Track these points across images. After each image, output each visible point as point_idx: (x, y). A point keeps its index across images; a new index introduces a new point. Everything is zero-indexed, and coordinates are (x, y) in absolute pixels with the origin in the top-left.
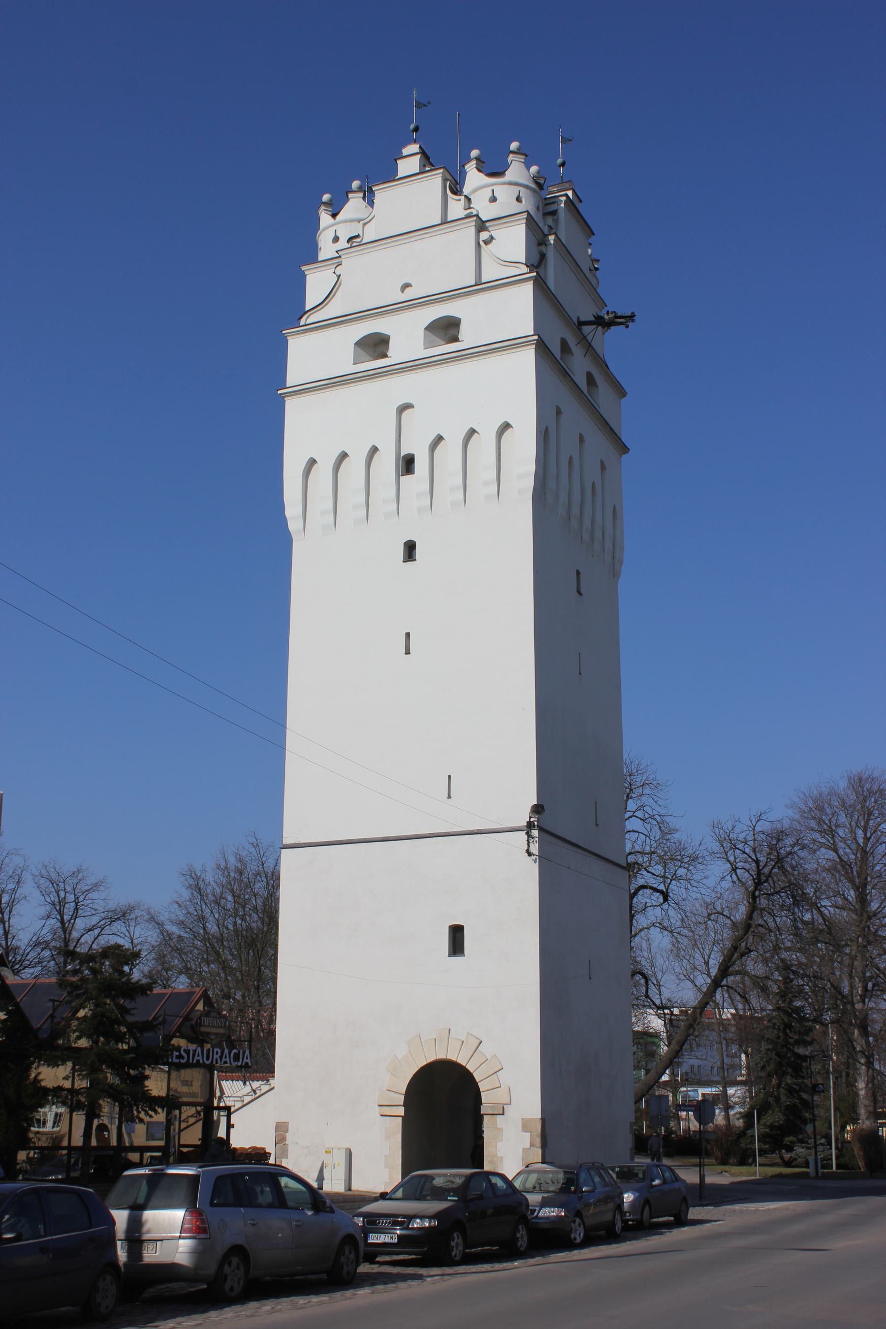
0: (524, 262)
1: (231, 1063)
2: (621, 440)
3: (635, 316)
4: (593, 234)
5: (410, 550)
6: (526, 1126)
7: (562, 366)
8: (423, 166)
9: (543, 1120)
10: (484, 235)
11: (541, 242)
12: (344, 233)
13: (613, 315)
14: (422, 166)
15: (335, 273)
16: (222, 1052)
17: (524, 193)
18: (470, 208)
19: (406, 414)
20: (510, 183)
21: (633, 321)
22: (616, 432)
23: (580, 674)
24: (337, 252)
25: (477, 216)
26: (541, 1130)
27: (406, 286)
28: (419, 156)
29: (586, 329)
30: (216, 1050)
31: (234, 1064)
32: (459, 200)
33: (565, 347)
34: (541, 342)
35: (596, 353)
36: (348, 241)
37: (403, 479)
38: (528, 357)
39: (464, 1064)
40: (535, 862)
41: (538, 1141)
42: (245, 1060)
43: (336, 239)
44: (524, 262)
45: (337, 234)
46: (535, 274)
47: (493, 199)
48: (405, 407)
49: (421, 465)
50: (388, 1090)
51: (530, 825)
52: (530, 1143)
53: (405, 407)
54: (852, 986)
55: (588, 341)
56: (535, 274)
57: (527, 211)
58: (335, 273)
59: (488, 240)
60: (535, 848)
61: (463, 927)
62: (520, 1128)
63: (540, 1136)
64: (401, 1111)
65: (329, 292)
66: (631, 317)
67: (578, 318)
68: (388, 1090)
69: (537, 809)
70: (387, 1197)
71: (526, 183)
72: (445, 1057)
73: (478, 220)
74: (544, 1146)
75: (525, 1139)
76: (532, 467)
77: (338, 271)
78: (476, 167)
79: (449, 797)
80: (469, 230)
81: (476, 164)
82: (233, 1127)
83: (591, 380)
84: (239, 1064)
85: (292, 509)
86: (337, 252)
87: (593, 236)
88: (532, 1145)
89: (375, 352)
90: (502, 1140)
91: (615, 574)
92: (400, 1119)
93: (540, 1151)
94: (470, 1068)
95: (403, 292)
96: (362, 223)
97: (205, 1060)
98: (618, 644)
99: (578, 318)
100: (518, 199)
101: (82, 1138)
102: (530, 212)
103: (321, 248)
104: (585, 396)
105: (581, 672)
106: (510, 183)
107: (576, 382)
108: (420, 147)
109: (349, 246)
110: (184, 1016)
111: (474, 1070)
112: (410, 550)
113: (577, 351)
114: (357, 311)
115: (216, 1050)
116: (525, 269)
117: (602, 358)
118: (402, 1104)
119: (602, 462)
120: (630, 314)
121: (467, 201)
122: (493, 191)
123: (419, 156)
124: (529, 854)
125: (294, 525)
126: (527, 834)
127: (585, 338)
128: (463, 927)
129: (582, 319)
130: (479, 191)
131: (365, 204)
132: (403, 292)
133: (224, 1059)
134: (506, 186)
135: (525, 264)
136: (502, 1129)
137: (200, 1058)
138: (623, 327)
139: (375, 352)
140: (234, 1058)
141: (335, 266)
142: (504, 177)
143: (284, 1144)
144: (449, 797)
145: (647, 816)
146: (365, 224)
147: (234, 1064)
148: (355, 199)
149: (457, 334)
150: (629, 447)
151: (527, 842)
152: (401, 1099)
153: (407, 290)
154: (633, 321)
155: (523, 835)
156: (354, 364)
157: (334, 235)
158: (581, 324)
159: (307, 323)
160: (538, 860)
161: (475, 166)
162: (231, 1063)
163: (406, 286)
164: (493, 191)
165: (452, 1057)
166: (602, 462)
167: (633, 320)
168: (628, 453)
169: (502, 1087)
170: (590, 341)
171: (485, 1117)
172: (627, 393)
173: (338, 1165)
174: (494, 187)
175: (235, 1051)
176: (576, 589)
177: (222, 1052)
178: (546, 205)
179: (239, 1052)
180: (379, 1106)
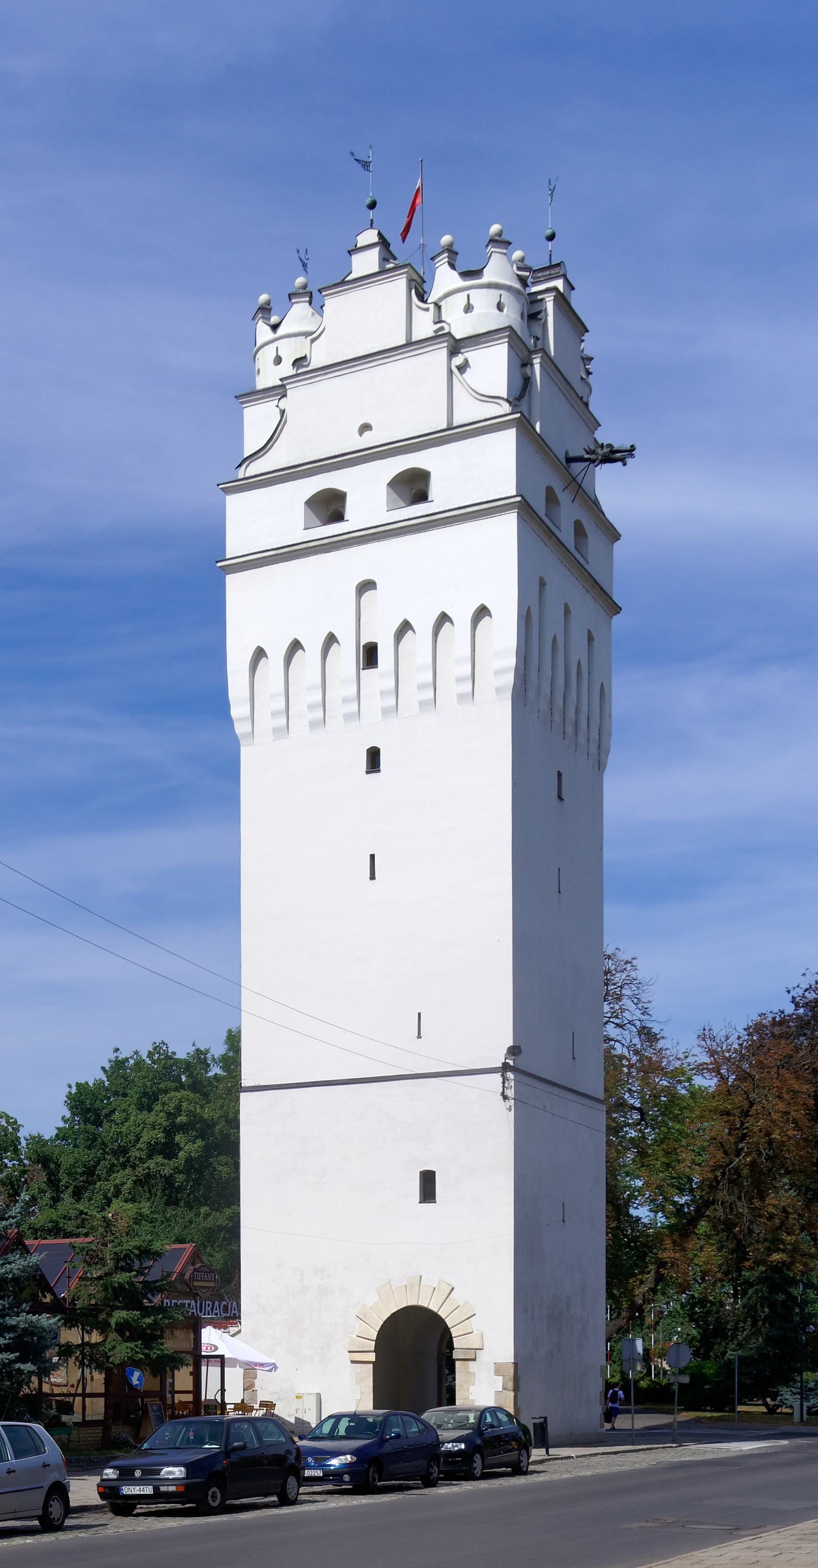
0: (506, 397)
1: (221, 1315)
2: (611, 598)
3: (634, 449)
4: (587, 331)
5: (374, 759)
6: (499, 1369)
7: (547, 527)
8: (384, 260)
9: (516, 1364)
10: (458, 360)
11: (525, 362)
12: (290, 350)
13: (609, 449)
14: (382, 260)
15: (277, 406)
16: (213, 1305)
17: (506, 297)
18: (440, 321)
19: (368, 596)
20: (490, 286)
21: (632, 456)
22: (606, 590)
23: (559, 892)
24: (281, 380)
25: (449, 334)
26: (514, 1373)
27: (365, 428)
28: (376, 251)
29: (577, 467)
30: (207, 1302)
31: (224, 1315)
32: (427, 310)
33: (551, 497)
34: (524, 503)
35: (586, 494)
36: (294, 364)
37: (364, 673)
38: (509, 522)
39: (436, 1310)
40: (510, 1110)
41: (510, 1385)
42: (233, 1312)
43: (278, 360)
44: (506, 397)
45: (279, 354)
46: (518, 415)
47: (468, 308)
48: (366, 586)
49: (385, 655)
50: (357, 1336)
51: (505, 1067)
52: (503, 1386)
53: (366, 586)
54: (781, 1298)
55: (578, 483)
56: (518, 415)
57: (510, 328)
58: (277, 406)
59: (463, 365)
60: (510, 1093)
61: (434, 1172)
62: (493, 1372)
63: (512, 1379)
64: (372, 1357)
65: (273, 432)
66: (633, 448)
67: (567, 452)
68: (357, 1336)
69: (514, 1051)
70: (442, 1428)
71: (508, 282)
72: (416, 1304)
73: (451, 339)
74: (516, 1389)
75: (499, 1382)
76: (511, 661)
77: (283, 404)
78: (448, 262)
79: (419, 1037)
80: (441, 353)
81: (448, 257)
82: (190, 1372)
83: (579, 530)
84: (228, 1315)
85: (238, 710)
86: (281, 380)
87: (586, 334)
88: (504, 1388)
89: (328, 510)
90: (474, 1384)
91: (600, 766)
92: (371, 1366)
93: (512, 1394)
94: (442, 1314)
95: (361, 435)
96: (309, 338)
97: (199, 1313)
98: (601, 849)
99: (567, 452)
100: (500, 307)
101: (104, 1385)
102: (514, 327)
103: (259, 370)
104: (571, 554)
105: (561, 891)
106: (490, 286)
107: (563, 541)
108: (380, 235)
109: (294, 372)
110: (178, 1271)
111: (446, 1316)
112: (374, 759)
113: (564, 498)
114: (307, 461)
115: (207, 1302)
116: (506, 408)
117: (593, 497)
118: (373, 1349)
119: (589, 632)
120: (629, 448)
121: (437, 309)
122: (468, 296)
123: (376, 251)
124: (505, 1097)
125: (240, 729)
126: (502, 1076)
127: (574, 479)
128: (434, 1172)
129: (572, 454)
130: (452, 297)
131: (311, 310)
132: (361, 435)
133: (215, 1311)
134: (484, 291)
135: (507, 401)
136: (474, 1373)
137: (194, 1311)
138: (620, 464)
139: (328, 510)
140: (223, 1310)
141: (279, 397)
142: (481, 279)
143: (253, 1391)
144: (419, 1037)
145: (626, 1022)
146: (313, 341)
147: (224, 1315)
148: (299, 304)
149: (424, 488)
150: (620, 606)
151: (502, 1085)
152: (372, 1345)
153: (367, 434)
154: (632, 456)
155: (497, 1078)
156: (305, 529)
157: (275, 355)
158: (570, 460)
159: (247, 475)
160: (513, 1108)
161: (446, 260)
162: (221, 1315)
163: (365, 428)
164: (468, 296)
165: (424, 1303)
166: (589, 632)
167: (633, 455)
168: (619, 613)
169: (474, 1333)
170: (580, 483)
171: (457, 1363)
172: (620, 536)
173: (309, 1409)
174: (471, 292)
175: (225, 1303)
176: (557, 795)
177: (213, 1305)
178: (532, 303)
179: (228, 1303)
180: (350, 1352)
